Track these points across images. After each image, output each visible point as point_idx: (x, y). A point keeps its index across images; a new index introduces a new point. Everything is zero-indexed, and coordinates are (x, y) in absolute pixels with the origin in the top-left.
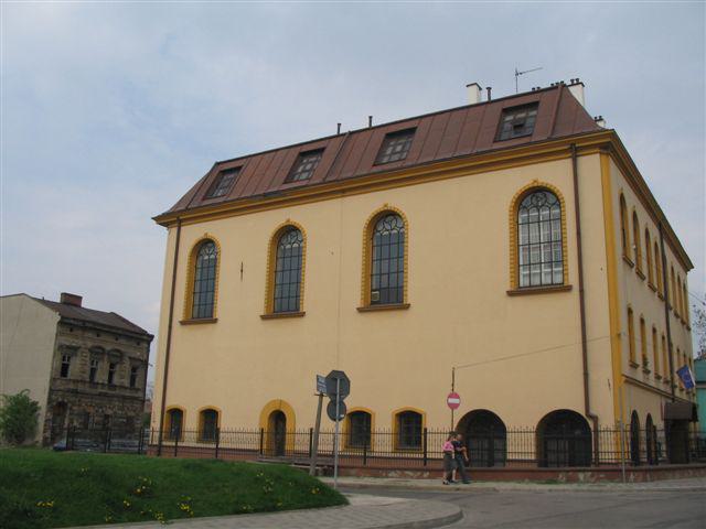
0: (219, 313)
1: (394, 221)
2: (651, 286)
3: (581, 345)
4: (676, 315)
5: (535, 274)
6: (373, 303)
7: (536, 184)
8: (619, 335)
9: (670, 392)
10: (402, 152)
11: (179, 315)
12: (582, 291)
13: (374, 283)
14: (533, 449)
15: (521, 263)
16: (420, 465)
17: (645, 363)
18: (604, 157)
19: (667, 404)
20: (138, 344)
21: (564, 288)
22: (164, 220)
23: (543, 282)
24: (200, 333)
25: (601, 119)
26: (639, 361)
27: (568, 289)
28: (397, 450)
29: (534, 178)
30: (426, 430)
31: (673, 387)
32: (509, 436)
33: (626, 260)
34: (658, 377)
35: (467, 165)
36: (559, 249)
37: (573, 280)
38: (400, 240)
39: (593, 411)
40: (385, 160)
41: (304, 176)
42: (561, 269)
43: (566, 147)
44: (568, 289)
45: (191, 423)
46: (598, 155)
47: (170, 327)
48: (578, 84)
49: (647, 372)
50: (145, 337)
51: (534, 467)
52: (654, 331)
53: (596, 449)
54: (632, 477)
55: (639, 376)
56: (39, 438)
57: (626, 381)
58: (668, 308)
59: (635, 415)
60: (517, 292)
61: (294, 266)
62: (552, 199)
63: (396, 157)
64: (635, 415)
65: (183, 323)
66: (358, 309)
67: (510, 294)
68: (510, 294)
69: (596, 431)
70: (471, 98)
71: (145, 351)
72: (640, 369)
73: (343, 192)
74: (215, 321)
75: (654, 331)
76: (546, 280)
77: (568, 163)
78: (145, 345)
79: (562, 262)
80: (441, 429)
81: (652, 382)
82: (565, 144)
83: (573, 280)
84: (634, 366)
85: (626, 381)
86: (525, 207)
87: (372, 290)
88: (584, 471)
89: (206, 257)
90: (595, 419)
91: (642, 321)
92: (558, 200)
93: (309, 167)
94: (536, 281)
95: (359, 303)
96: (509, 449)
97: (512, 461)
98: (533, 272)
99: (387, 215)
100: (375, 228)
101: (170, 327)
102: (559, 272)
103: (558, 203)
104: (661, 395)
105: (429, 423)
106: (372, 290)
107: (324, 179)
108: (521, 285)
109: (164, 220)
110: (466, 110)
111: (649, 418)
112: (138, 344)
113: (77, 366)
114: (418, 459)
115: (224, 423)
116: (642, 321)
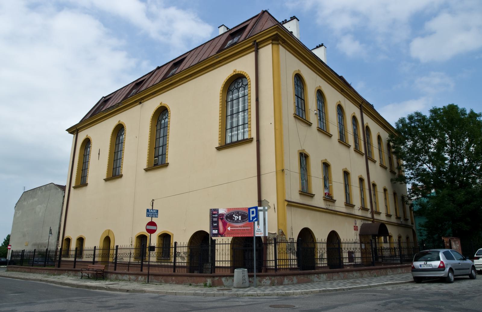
6: (155, 165)
11: (73, 184)
14: (228, 258)
18: (275, 46)
29: (234, 69)
30: (176, 243)
34: (388, 216)
43: (251, 44)
45: (73, 245)
46: (271, 45)
51: (184, 272)
57: (288, 205)
67: (218, 149)
68: (218, 149)
85: (288, 205)
97: (220, 267)
113: (363, 247)
114: (225, 267)
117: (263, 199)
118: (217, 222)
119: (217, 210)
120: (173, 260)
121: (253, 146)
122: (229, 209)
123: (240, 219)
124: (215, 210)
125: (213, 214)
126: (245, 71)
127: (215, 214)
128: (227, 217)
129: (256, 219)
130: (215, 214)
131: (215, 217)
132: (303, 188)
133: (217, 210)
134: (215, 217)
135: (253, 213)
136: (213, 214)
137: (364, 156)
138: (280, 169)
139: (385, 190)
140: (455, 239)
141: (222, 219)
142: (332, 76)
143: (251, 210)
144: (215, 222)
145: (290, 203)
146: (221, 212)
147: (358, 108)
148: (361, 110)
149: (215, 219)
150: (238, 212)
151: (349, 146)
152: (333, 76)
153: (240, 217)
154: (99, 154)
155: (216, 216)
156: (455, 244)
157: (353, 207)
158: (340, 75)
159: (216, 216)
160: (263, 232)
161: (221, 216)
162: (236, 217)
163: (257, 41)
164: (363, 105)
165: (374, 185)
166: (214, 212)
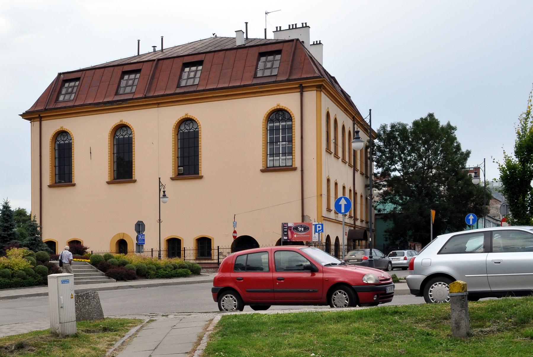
0: (76, 178)
1: (191, 124)
2: (344, 161)
3: (301, 201)
6: (179, 174)
7: (278, 107)
8: (321, 195)
9: (352, 222)
11: (47, 180)
12: (302, 171)
15: (268, 153)
18: (319, 93)
21: (291, 169)
22: (27, 115)
23: (281, 165)
24: (64, 192)
27: (295, 169)
28: (197, 259)
29: (278, 103)
30: (184, 248)
31: (355, 219)
34: (362, 221)
35: (244, 92)
37: (297, 164)
42: (291, 157)
43: (297, 86)
44: (295, 169)
46: (316, 91)
47: (41, 189)
48: (306, 26)
55: (332, 215)
59: (328, 238)
60: (266, 170)
64: (328, 238)
65: (50, 186)
66: (171, 178)
67: (262, 171)
77: (298, 94)
79: (291, 153)
83: (297, 164)
84: (329, 210)
85: (324, 220)
87: (179, 167)
92: (291, 116)
94: (276, 164)
95: (107, 179)
99: (122, 127)
100: (56, 139)
101: (41, 189)
102: (277, 160)
103: (290, 119)
105: (215, 245)
106: (179, 167)
107: (145, 95)
108: (268, 166)
109: (27, 115)
110: (102, 70)
111: (337, 239)
117: (305, 214)
118: (287, 232)
119: (287, 224)
120: (216, 257)
122: (295, 224)
123: (303, 230)
124: (285, 224)
125: (284, 226)
126: (289, 108)
127: (285, 226)
128: (294, 229)
129: (322, 231)
130: (285, 226)
131: (285, 228)
132: (328, 207)
133: (287, 224)
134: (285, 228)
135: (319, 227)
136: (284, 226)
137: (353, 168)
138: (319, 194)
139: (361, 196)
140: (418, 244)
141: (290, 230)
142: (343, 101)
143: (318, 226)
144: (286, 232)
145: (325, 218)
146: (290, 225)
147: (351, 119)
148: (353, 121)
149: (285, 230)
150: (301, 225)
151: (338, 158)
152: (342, 100)
153: (303, 228)
154: (91, 153)
155: (286, 227)
156: (418, 247)
157: (330, 211)
158: (332, 75)
159: (286, 227)
160: (317, 238)
161: (289, 228)
162: (300, 229)
163: (303, 85)
164: (356, 117)
165: (356, 193)
166: (285, 225)
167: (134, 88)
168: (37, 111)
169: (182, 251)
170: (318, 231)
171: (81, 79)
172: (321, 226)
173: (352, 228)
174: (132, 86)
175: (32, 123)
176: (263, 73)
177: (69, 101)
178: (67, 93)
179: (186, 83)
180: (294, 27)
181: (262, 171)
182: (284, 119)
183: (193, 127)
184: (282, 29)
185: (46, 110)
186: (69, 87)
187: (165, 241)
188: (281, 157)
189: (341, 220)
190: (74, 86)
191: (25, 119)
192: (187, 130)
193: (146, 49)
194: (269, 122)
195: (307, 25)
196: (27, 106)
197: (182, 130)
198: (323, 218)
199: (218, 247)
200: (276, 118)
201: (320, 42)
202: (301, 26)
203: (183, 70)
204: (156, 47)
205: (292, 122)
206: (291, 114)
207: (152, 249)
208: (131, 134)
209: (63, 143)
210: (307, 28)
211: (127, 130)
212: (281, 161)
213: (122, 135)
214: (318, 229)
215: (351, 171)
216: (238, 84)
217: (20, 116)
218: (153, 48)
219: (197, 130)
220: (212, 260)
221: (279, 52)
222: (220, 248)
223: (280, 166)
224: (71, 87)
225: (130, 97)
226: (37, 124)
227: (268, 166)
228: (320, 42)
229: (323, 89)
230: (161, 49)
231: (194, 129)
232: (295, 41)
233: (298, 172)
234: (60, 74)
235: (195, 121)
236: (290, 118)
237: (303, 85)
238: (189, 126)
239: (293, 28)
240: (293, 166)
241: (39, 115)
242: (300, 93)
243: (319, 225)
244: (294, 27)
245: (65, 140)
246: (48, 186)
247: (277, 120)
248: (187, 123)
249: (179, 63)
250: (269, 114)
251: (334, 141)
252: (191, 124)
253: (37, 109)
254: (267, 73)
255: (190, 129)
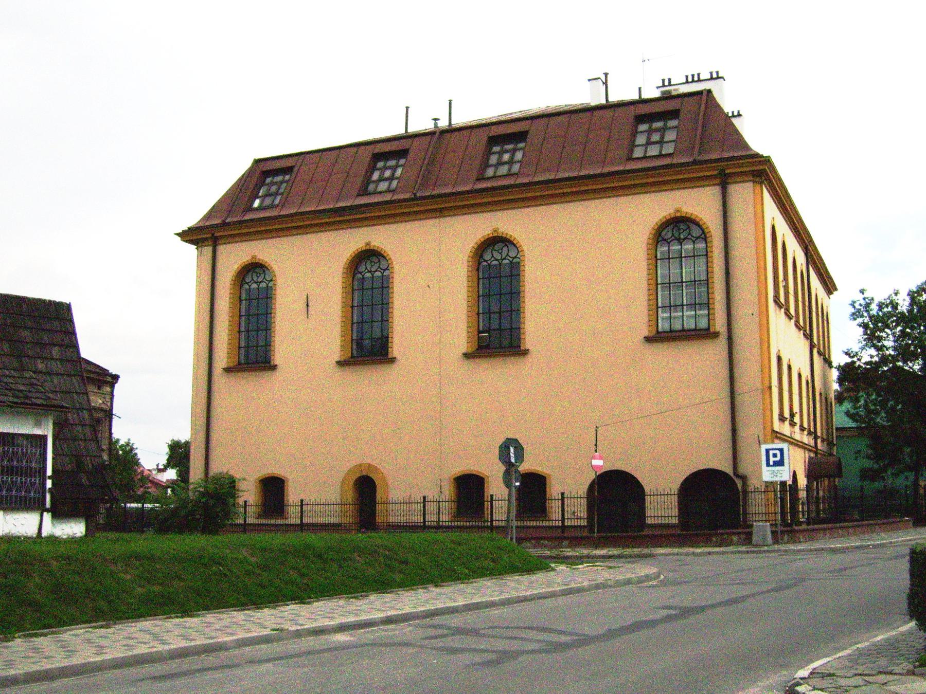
1: (505, 249)
2: (797, 325)
4: (819, 353)
5: (675, 318)
6: (480, 348)
7: (678, 215)
9: (812, 443)
10: (511, 162)
11: (222, 359)
12: (730, 339)
13: (481, 324)
14: (675, 512)
15: (660, 305)
16: (558, 533)
17: (792, 415)
18: (758, 186)
19: (810, 458)
20: (99, 388)
21: (706, 334)
22: (191, 236)
23: (686, 327)
25: (739, 115)
26: (787, 414)
27: (716, 335)
29: (677, 206)
30: (492, 496)
32: (648, 498)
33: (776, 301)
36: (704, 289)
37: (720, 324)
38: (514, 271)
39: (741, 470)
40: (490, 172)
41: (383, 186)
43: (715, 173)
44: (716, 335)
48: (718, 78)
49: (793, 424)
50: (109, 379)
52: (800, 376)
53: (745, 510)
54: (786, 538)
56: (882, 483)
58: (812, 347)
60: (657, 338)
61: (378, 299)
62: (696, 232)
63: (504, 170)
66: (464, 354)
67: (649, 340)
69: (745, 492)
70: (592, 97)
71: (108, 397)
72: (787, 423)
73: (441, 212)
74: (274, 368)
75: (800, 376)
76: (690, 324)
78: (108, 389)
79: (708, 305)
80: (667, 490)
81: (797, 436)
82: (714, 169)
83: (720, 324)
86: (665, 240)
88: (739, 533)
89: (254, 286)
90: (744, 478)
91: (790, 368)
92: (703, 232)
93: (388, 174)
94: (677, 326)
95: (337, 357)
96: (648, 513)
98: (673, 315)
99: (497, 241)
103: (704, 236)
104: (805, 448)
105: (554, 489)
106: (479, 332)
108: (660, 329)
109: (191, 236)
112: (99, 388)
115: (293, 496)
116: (790, 368)
121: (714, 352)
143: (771, 453)
167: (395, 183)
168: (207, 227)
169: (486, 503)
170: (771, 463)
171: (296, 169)
172: (778, 452)
173: (812, 455)
174: (391, 179)
175: (200, 249)
176: (646, 151)
177: (272, 207)
178: (266, 196)
179: (495, 172)
180: (696, 79)
181: (649, 340)
182: (689, 237)
183: (508, 255)
184: (672, 83)
185: (224, 224)
186: (273, 184)
187: (452, 480)
188: (686, 313)
189: (787, 434)
190: (282, 182)
191: (186, 241)
192: (496, 260)
193: (420, 124)
194: (660, 243)
195: (720, 76)
196: (193, 217)
197: (486, 261)
198: (774, 435)
199: (563, 494)
200: (673, 235)
201: (739, 112)
202: (709, 77)
203: (488, 153)
204: (438, 119)
205: (706, 243)
206: (704, 227)
207: (424, 498)
208: (387, 269)
209: (257, 286)
210: (719, 80)
211: (379, 261)
212: (688, 319)
213: (370, 272)
214: (772, 459)
215: (807, 344)
216: (598, 171)
217: (177, 236)
218: (434, 121)
219: (515, 260)
220: (549, 520)
221: (674, 114)
222: (565, 496)
223: (671, 331)
224: (276, 183)
225: (388, 197)
226: (208, 250)
227: (660, 329)
228: (739, 112)
229: (766, 180)
230: (448, 124)
231: (511, 259)
232: (705, 94)
233: (722, 342)
234: (258, 162)
235: (511, 242)
236: (703, 236)
237: (726, 172)
238: (500, 253)
239: (693, 81)
240: (712, 330)
241: (213, 235)
242: (720, 186)
243: (775, 452)
244: (696, 79)
245: (259, 280)
246: (224, 369)
247: (676, 239)
248: (496, 247)
249: (481, 138)
250: (658, 229)
251: (784, 283)
252: (505, 249)
253: (208, 223)
254: (653, 151)
255: (502, 260)
